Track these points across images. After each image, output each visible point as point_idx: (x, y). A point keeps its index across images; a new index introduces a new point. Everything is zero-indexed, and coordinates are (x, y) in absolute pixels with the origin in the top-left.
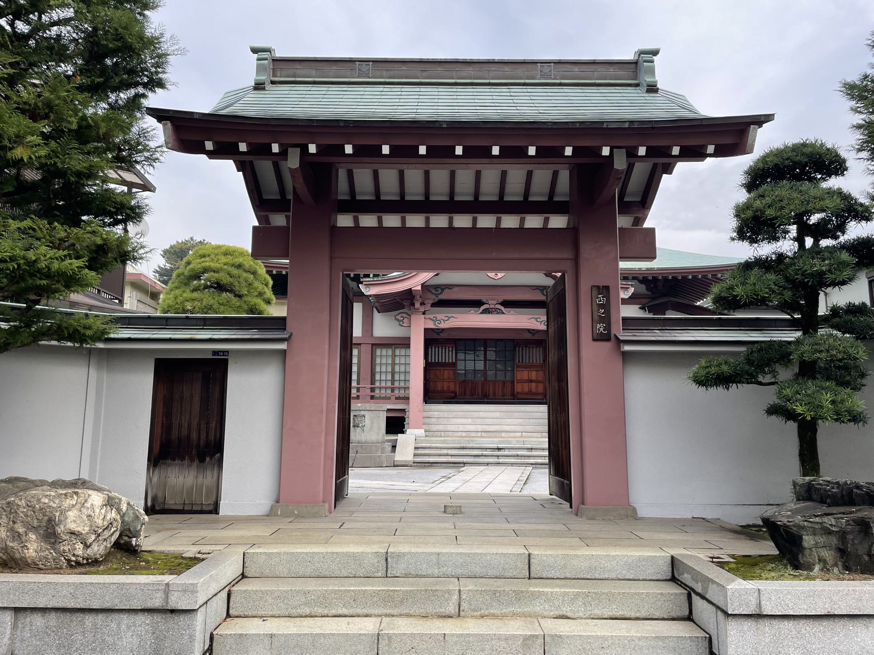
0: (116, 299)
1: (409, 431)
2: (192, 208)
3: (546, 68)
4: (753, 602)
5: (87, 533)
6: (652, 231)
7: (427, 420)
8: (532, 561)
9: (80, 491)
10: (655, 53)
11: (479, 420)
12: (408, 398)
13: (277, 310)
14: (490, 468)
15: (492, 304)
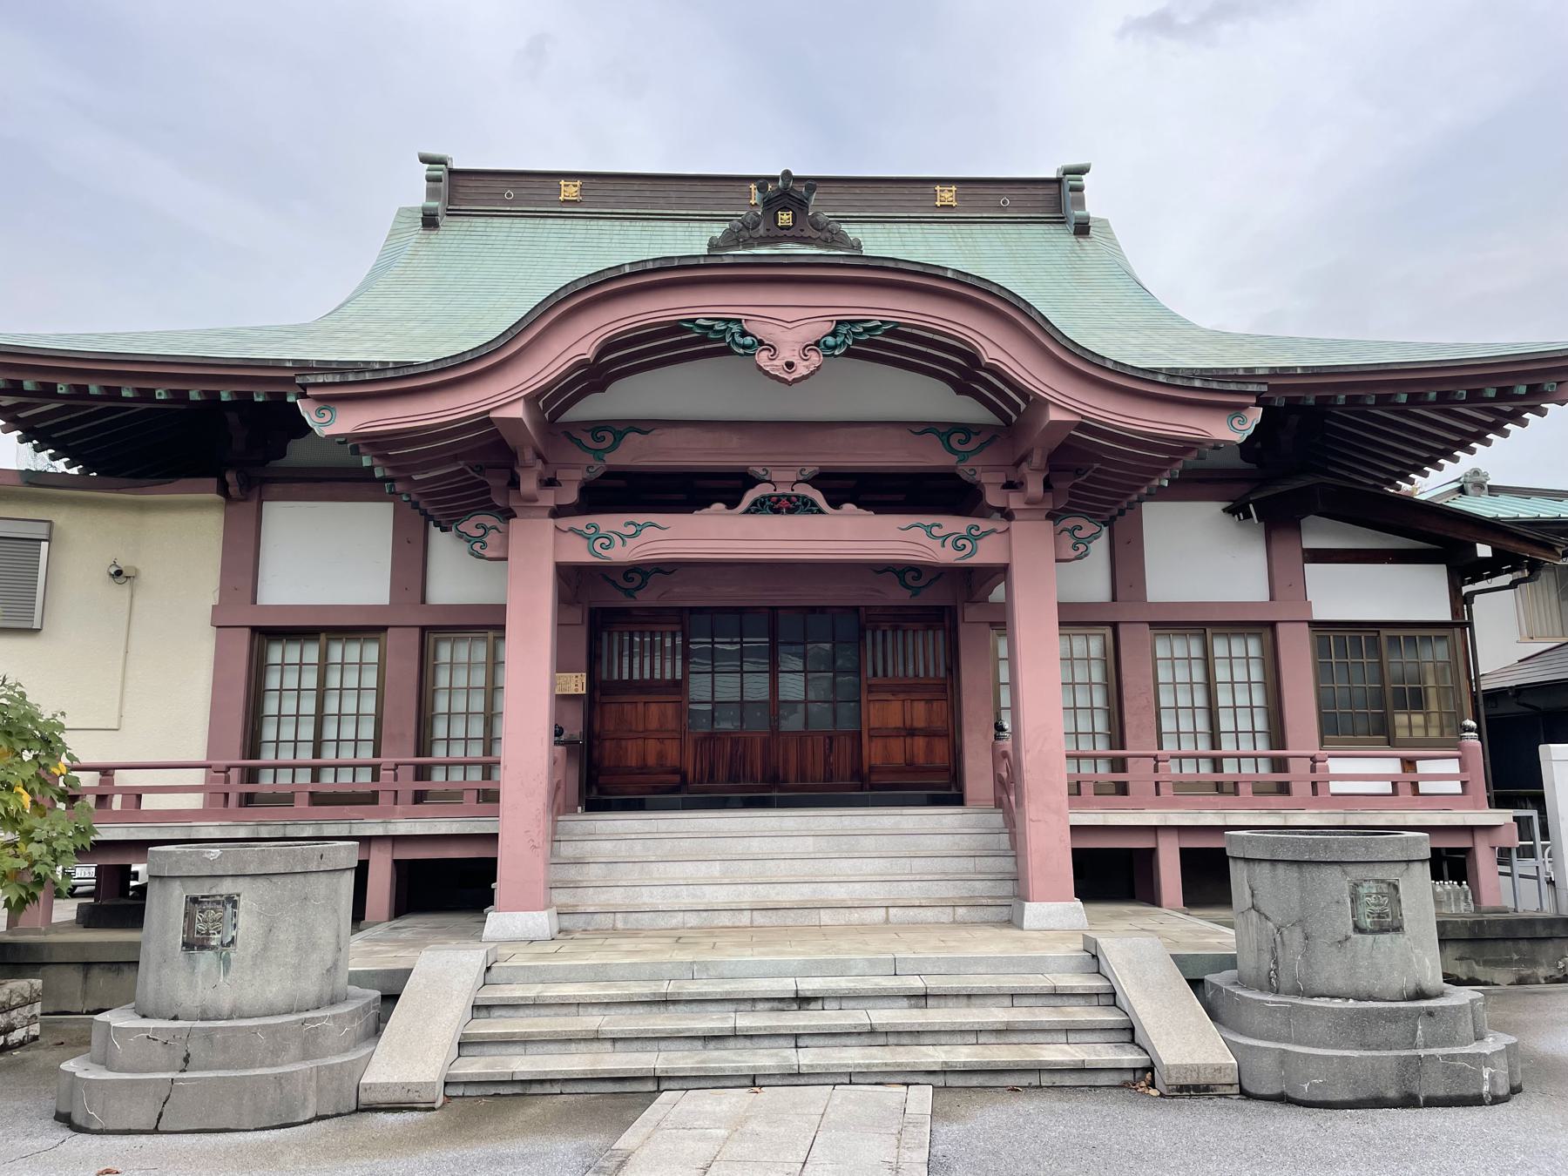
1: (496, 921)
7: (572, 873)
10: (1083, 170)
11: (747, 866)
15: (784, 481)
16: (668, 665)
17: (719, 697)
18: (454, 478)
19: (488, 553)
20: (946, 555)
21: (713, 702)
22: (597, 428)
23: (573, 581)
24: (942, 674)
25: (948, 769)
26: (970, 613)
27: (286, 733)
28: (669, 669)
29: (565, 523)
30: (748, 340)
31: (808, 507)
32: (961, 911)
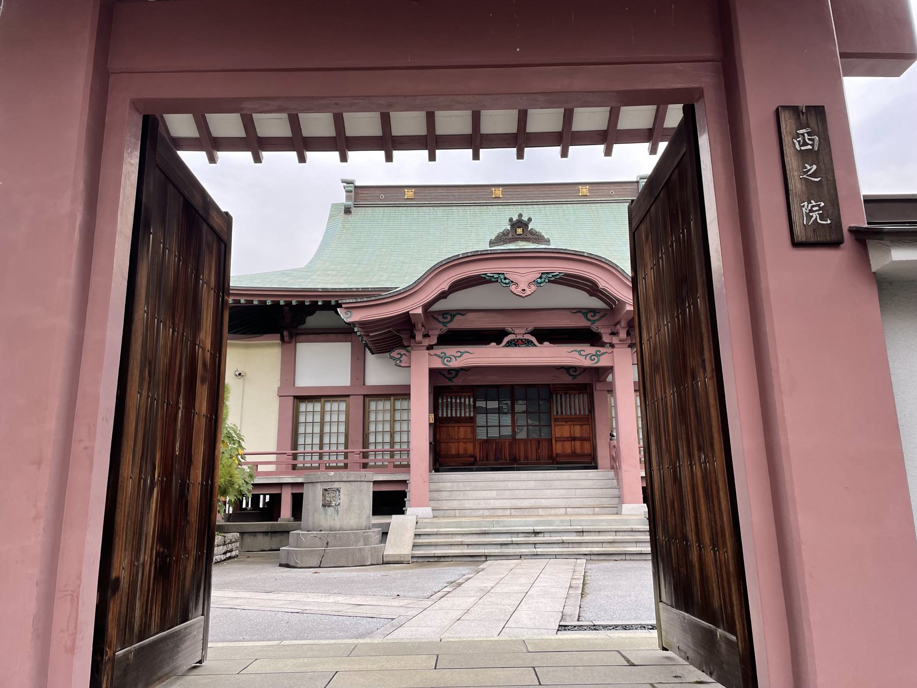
1: (409, 510)
7: (436, 495)
12: (408, 466)
14: (525, 562)
15: (520, 333)
16: (449, 412)
18: (393, 336)
19: (402, 364)
20: (587, 363)
22: (444, 313)
23: (434, 373)
24: (587, 413)
25: (590, 455)
26: (599, 386)
27: (308, 441)
28: (467, 413)
29: (432, 352)
30: (507, 281)
31: (529, 343)
32: (597, 509)
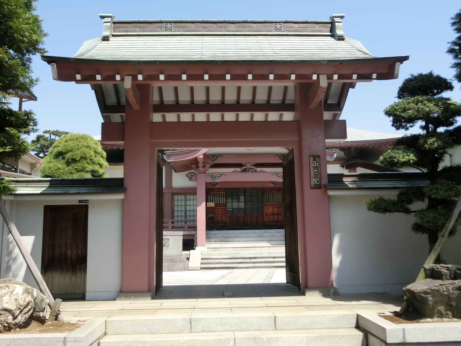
0: (14, 168)
2: (65, 113)
3: (278, 26)
4: (401, 335)
5: (15, 310)
6: (344, 122)
8: (277, 320)
9: (10, 285)
13: (116, 172)
17: (233, 207)
21: (232, 208)
